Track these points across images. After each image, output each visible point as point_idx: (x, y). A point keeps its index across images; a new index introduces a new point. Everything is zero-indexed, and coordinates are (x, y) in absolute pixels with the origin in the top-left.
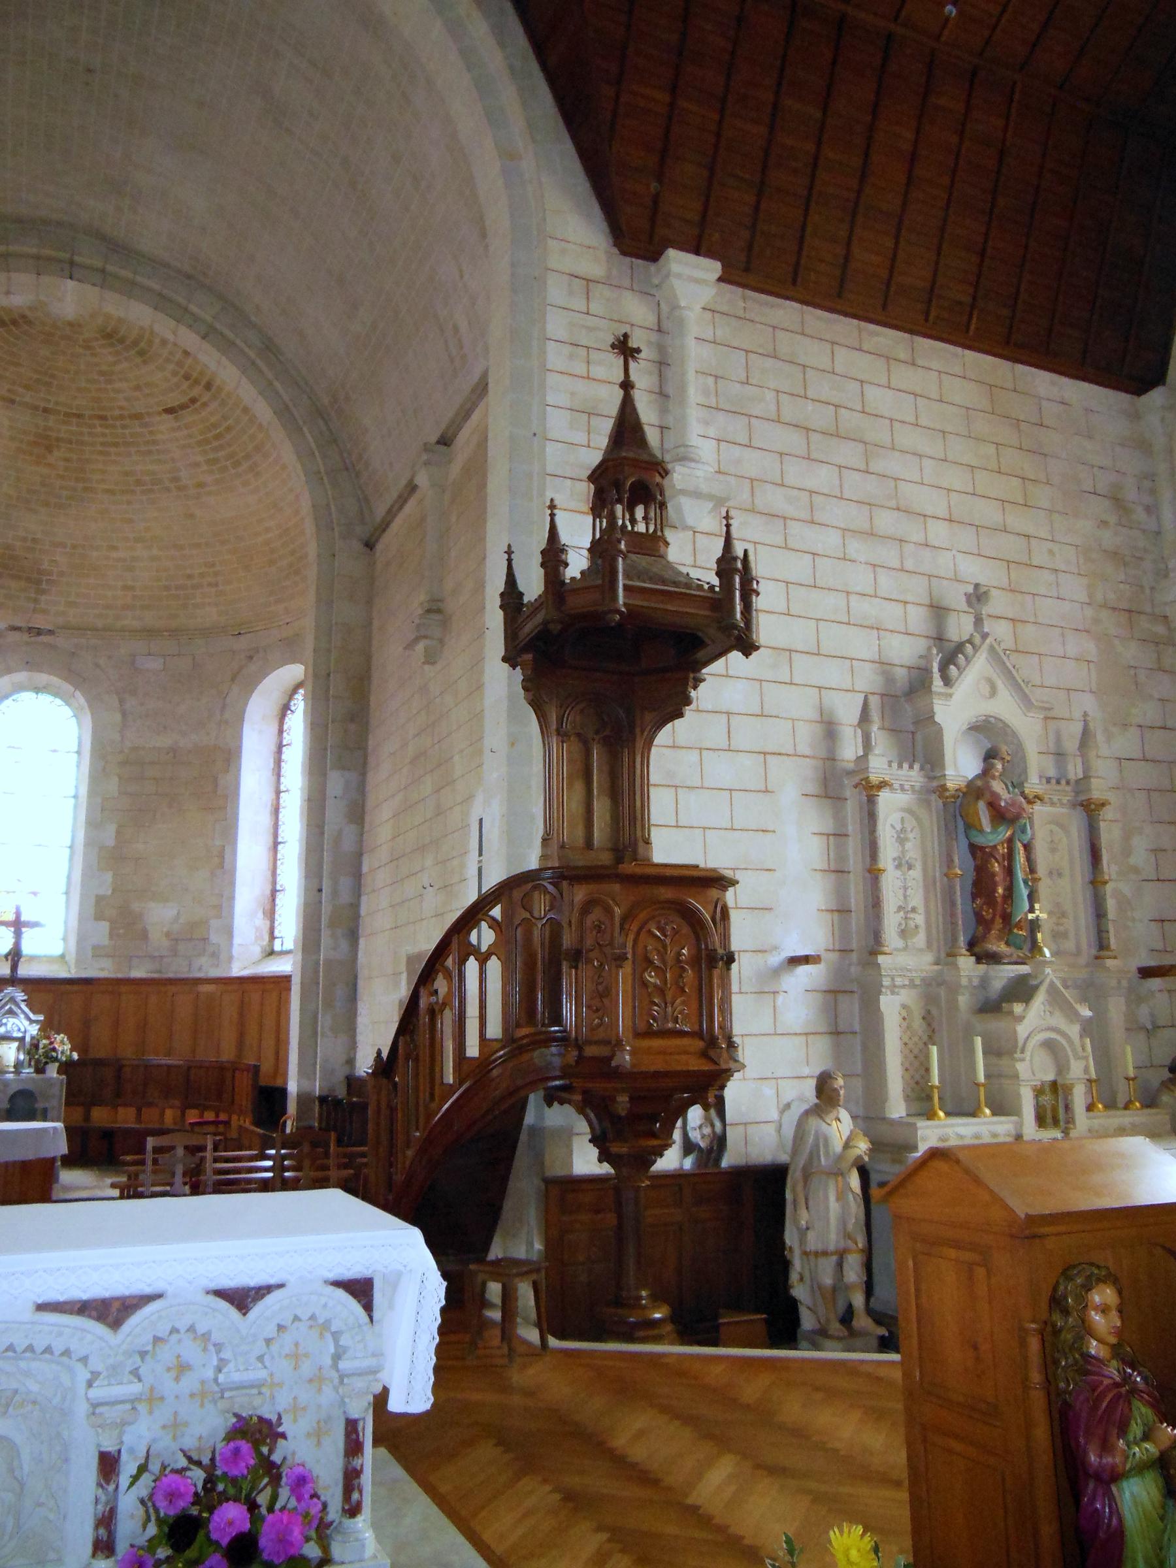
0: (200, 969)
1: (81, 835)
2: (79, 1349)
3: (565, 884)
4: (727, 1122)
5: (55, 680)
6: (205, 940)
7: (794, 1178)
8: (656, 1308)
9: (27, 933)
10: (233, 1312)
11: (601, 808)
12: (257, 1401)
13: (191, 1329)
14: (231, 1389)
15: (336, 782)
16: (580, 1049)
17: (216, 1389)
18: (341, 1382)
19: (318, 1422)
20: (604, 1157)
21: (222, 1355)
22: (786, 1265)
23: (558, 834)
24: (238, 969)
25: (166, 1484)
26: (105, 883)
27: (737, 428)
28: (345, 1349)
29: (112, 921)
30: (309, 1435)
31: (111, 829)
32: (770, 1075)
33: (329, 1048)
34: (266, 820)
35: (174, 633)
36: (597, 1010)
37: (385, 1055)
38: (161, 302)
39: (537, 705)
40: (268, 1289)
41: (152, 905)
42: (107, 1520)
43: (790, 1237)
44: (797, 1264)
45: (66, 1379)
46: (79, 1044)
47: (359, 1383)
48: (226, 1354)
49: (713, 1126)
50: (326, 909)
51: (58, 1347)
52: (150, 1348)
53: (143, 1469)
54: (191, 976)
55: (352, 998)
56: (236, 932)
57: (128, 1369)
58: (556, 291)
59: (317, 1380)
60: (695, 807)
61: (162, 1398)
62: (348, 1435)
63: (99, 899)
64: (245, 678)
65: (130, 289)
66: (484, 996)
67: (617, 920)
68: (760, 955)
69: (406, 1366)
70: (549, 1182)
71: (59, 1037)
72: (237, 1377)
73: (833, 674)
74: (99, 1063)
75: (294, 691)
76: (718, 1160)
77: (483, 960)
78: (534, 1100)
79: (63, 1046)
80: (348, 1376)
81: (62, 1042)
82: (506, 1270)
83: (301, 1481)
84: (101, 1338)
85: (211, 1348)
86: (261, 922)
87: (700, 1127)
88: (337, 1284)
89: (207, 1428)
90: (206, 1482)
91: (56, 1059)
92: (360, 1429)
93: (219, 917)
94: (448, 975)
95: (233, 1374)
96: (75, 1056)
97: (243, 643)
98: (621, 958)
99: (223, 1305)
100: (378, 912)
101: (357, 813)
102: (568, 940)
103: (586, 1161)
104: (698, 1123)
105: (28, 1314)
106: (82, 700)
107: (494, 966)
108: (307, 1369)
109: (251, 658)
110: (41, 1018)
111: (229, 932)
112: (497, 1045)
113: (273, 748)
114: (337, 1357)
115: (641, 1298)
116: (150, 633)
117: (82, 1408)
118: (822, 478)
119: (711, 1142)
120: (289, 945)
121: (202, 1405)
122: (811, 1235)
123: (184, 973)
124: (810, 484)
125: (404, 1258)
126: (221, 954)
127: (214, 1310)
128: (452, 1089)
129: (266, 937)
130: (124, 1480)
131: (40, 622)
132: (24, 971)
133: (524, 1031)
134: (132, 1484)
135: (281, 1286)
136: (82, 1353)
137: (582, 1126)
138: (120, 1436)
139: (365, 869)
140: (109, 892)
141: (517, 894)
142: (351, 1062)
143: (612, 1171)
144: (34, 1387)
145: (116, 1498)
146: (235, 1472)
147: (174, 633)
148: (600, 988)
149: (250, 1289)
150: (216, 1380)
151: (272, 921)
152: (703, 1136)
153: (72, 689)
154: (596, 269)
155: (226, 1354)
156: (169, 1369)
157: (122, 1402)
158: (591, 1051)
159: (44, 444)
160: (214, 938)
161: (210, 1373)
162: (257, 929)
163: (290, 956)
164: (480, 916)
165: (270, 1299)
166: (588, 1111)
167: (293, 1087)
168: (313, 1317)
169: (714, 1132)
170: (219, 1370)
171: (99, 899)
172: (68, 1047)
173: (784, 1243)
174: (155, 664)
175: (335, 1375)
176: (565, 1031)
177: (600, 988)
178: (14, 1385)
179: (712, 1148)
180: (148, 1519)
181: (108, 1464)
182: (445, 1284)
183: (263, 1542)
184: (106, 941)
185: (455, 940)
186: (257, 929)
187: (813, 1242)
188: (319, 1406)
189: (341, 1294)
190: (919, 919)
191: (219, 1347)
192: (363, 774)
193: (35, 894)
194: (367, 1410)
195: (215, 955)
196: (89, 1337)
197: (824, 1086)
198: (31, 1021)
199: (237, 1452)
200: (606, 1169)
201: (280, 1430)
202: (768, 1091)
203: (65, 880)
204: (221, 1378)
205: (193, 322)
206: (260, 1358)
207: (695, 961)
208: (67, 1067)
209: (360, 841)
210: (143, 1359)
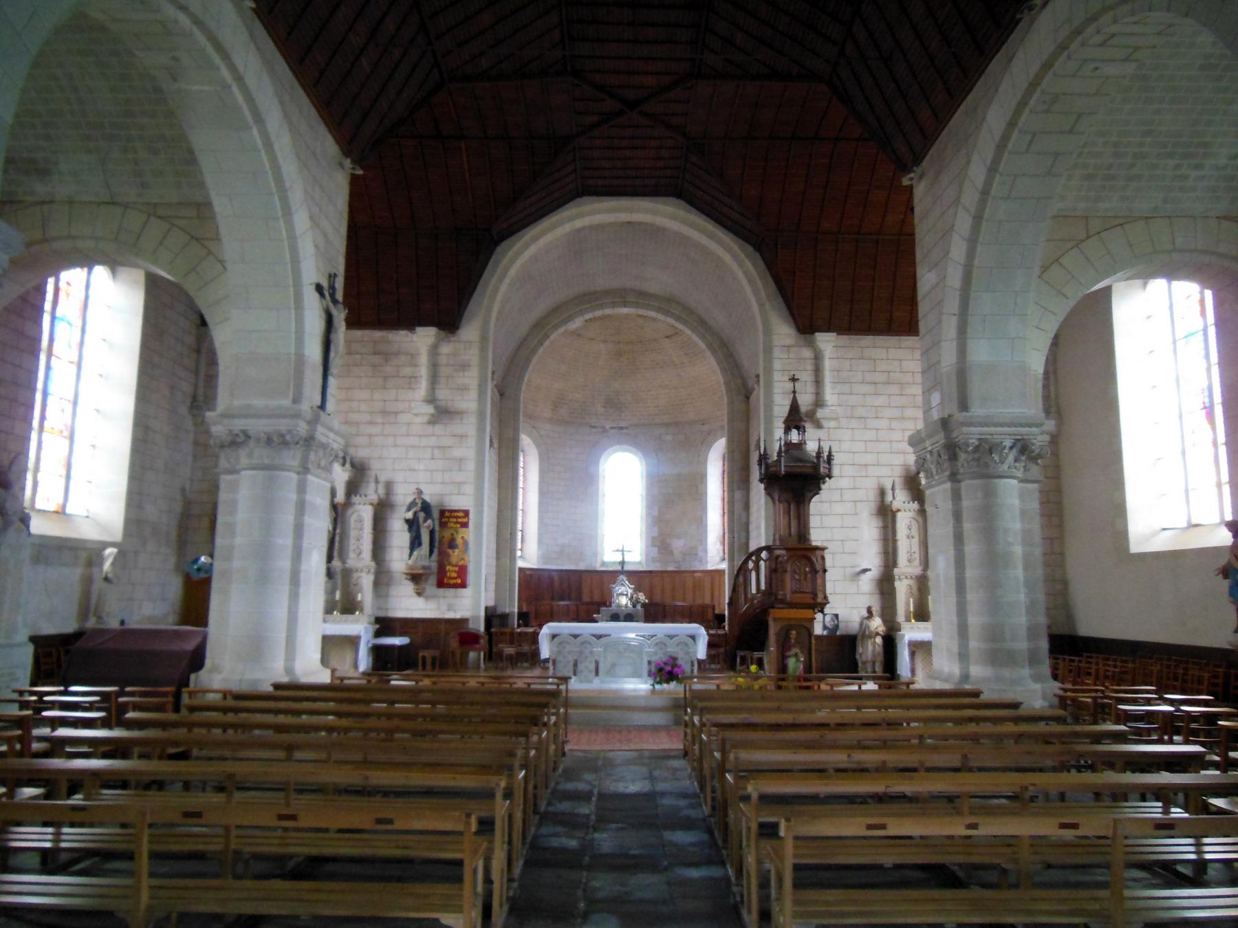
24: (710, 567)
27: (846, 388)
35: (676, 424)
38: (658, 310)
43: (858, 657)
46: (649, 596)
58: (777, 353)
60: (828, 521)
64: (707, 444)
65: (648, 307)
69: (701, 652)
73: (885, 471)
74: (656, 605)
79: (642, 597)
95: (669, 649)
97: (706, 428)
111: (705, 551)
116: (666, 425)
118: (880, 401)
124: (876, 404)
126: (703, 560)
131: (622, 424)
132: (627, 568)
147: (676, 424)
154: (790, 341)
159: (619, 354)
160: (700, 554)
171: (653, 538)
174: (669, 438)
181: (649, 663)
187: (864, 658)
190: (917, 556)
195: (701, 561)
197: (869, 610)
202: (855, 612)
205: (672, 315)
207: (811, 572)
208: (644, 605)
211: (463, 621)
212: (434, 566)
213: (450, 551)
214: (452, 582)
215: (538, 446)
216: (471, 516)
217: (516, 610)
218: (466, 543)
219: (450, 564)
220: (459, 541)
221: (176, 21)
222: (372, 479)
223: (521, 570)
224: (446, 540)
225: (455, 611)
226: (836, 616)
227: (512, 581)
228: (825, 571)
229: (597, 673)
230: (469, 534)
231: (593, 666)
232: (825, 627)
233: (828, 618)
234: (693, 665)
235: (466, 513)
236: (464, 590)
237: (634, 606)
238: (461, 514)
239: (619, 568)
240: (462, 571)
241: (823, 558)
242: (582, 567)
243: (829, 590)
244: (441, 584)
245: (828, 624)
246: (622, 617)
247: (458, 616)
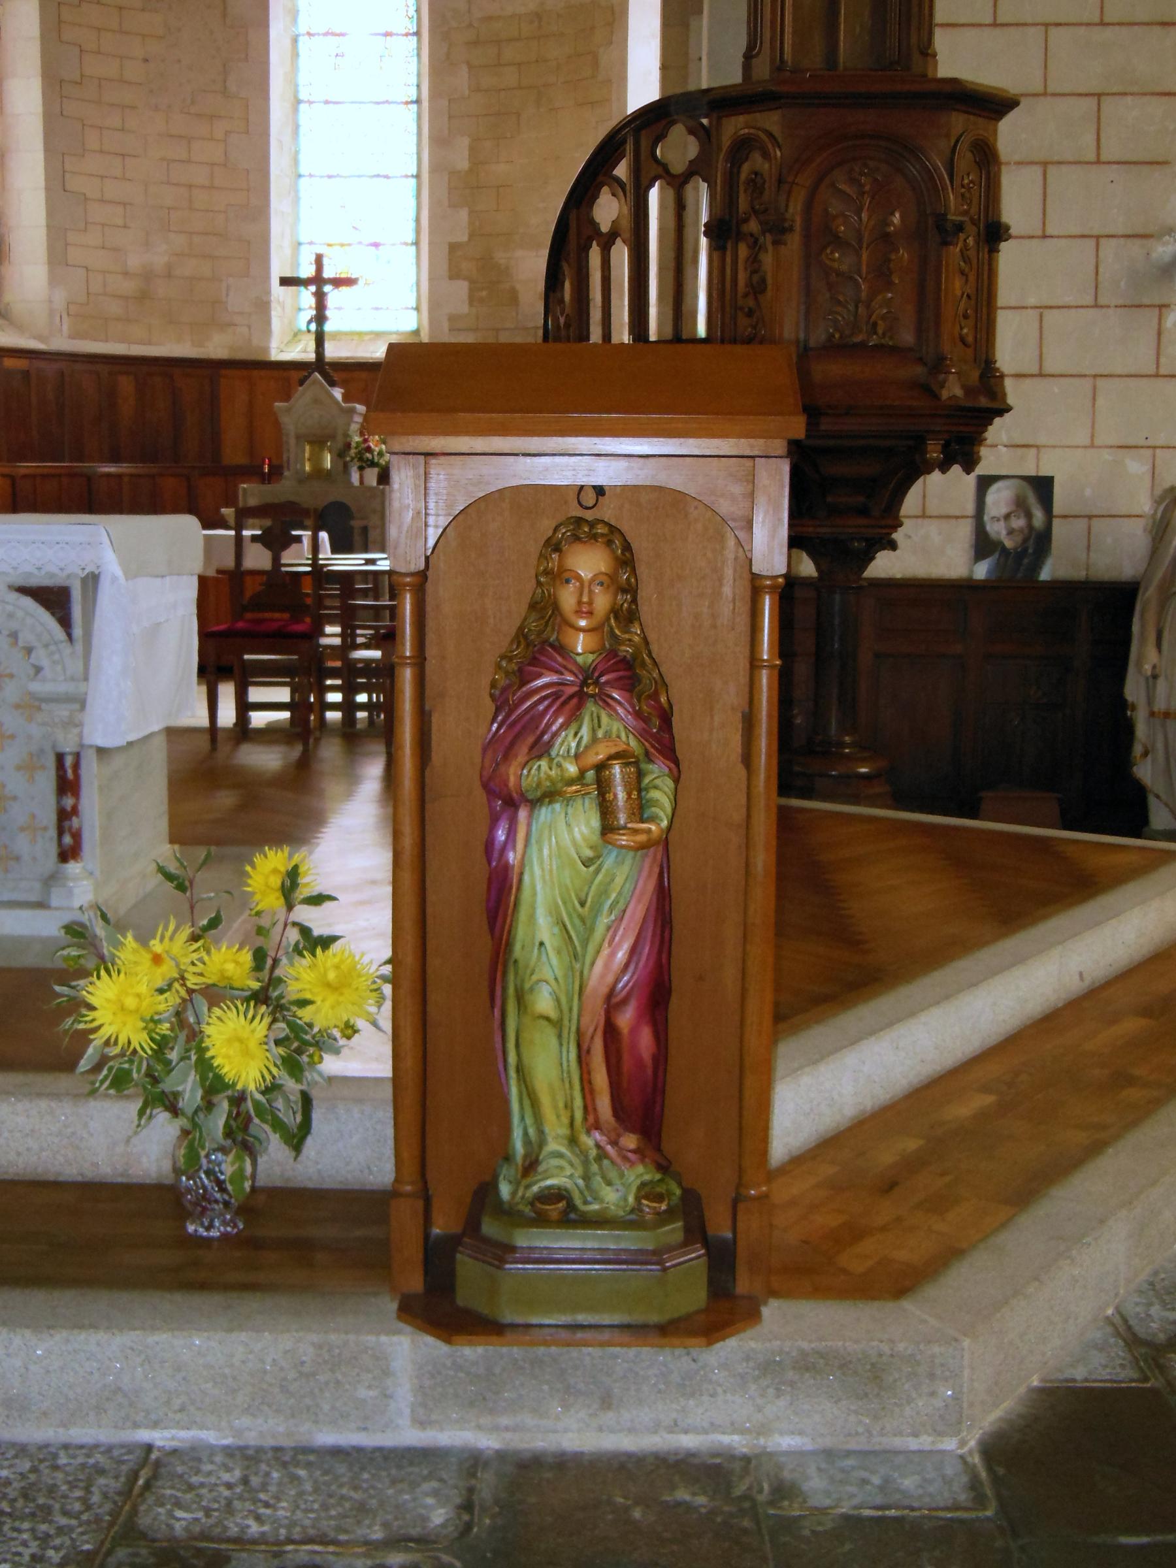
4: (1058, 508)
7: (1148, 596)
8: (863, 761)
22: (1129, 729)
26: (460, 226)
29: (472, 281)
31: (463, 144)
32: (1142, 442)
41: (519, 253)
43: (1133, 690)
44: (1141, 730)
49: (1029, 515)
63: (453, 247)
68: (1138, 242)
76: (1037, 565)
77: (607, 243)
87: (1007, 517)
88: (24, 590)
98: (779, 230)
104: (1004, 510)
115: (843, 745)
119: (1025, 540)
122: (1161, 686)
140: (465, 239)
152: (1011, 532)
164: (600, 178)
169: (1030, 526)
171: (453, 247)
173: (1126, 701)
179: (1025, 550)
184: (464, 309)
185: (573, 216)
189: (28, 602)
193: (376, 245)
202: (1136, 466)
203: (412, 225)
221: (694, 1494)
222: (856, 1512)
226: (1043, 486)
228: (995, 233)
232: (983, 545)
233: (999, 499)
241: (986, 158)
243: (1011, 349)
245: (996, 530)
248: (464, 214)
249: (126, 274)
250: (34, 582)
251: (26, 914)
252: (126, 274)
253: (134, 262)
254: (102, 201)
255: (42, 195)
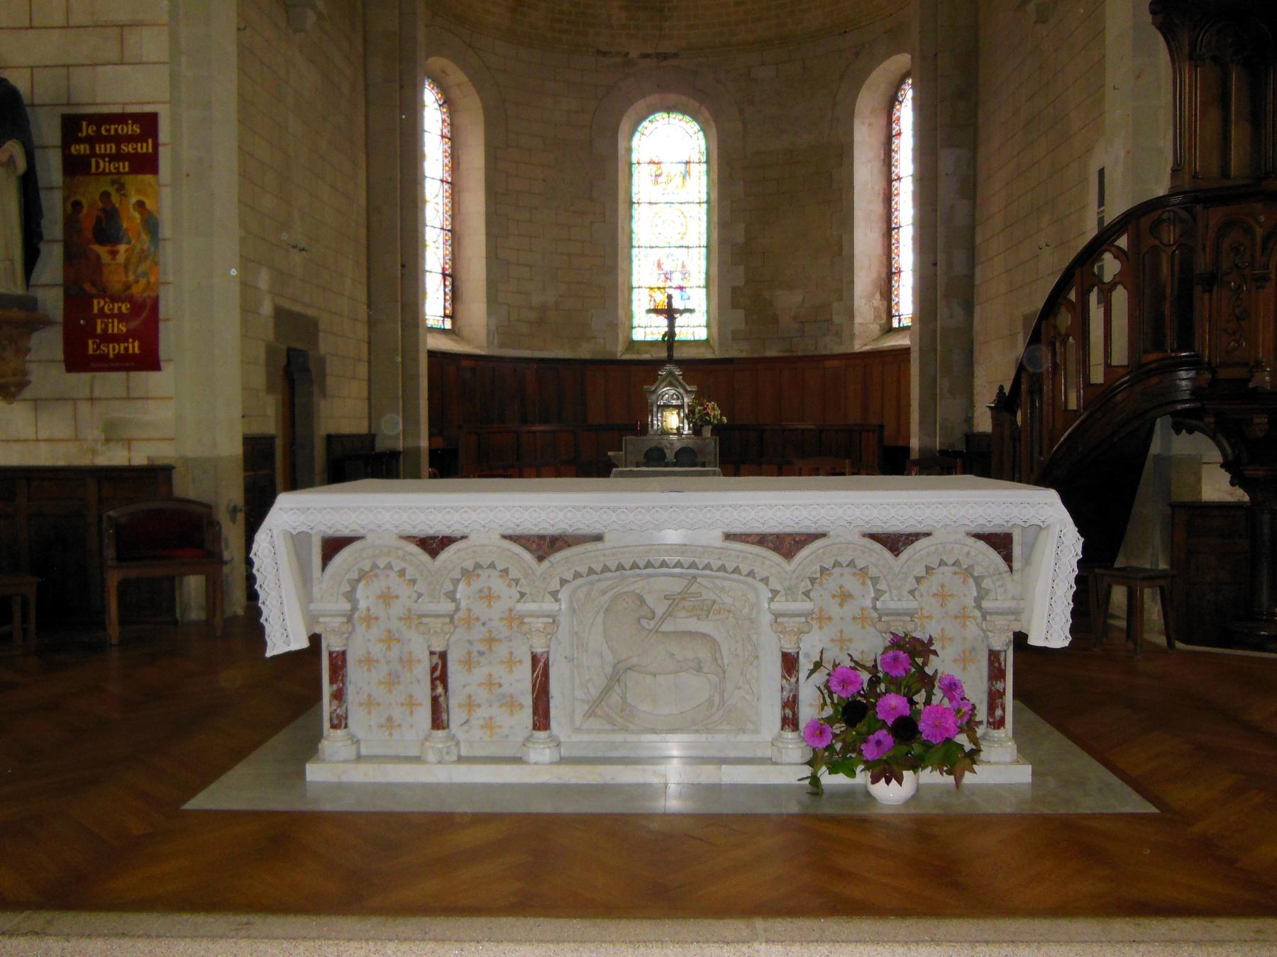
0: (825, 348)
1: (715, 235)
2: (761, 572)
3: (1199, 208)
5: (684, 99)
6: (830, 321)
9: (680, 320)
10: (887, 554)
11: (1239, 134)
12: (910, 627)
13: (851, 564)
14: (888, 615)
15: (948, 160)
16: (1214, 372)
17: (875, 615)
18: (984, 618)
19: (964, 652)
20: (1238, 479)
21: (878, 587)
23: (1190, 163)
24: (859, 346)
25: (839, 678)
28: (988, 592)
30: (955, 660)
31: (741, 227)
33: (948, 409)
34: (878, 208)
36: (1234, 333)
37: (1007, 391)
39: (1167, 30)
40: (916, 536)
42: (791, 704)
45: (751, 596)
47: (1000, 621)
48: (882, 586)
50: (941, 281)
51: (745, 569)
52: (818, 575)
53: (818, 665)
54: (816, 353)
55: (969, 363)
56: (856, 313)
57: (802, 590)
59: (962, 617)
61: (830, 619)
62: (991, 663)
66: (1110, 331)
67: (1259, 240)
70: (1176, 507)
71: (711, 405)
72: (892, 605)
75: (902, 81)
78: (1161, 426)
79: (714, 411)
80: (991, 614)
81: (713, 409)
82: (1131, 578)
83: (952, 687)
84: (779, 565)
85: (869, 582)
86: (877, 301)
88: (979, 536)
89: (869, 645)
90: (870, 680)
91: (709, 423)
92: (1002, 659)
93: (840, 299)
94: (1071, 307)
95: (889, 602)
96: (725, 420)
99: (877, 546)
100: (993, 280)
101: (970, 188)
102: (1202, 263)
103: (1217, 487)
105: (718, 542)
106: (707, 115)
107: (1120, 297)
108: (952, 606)
109: (857, 54)
110: (694, 388)
112: (1121, 371)
113: (881, 138)
114: (978, 600)
117: (766, 619)
120: (906, 322)
121: (863, 627)
123: (811, 352)
125: (1043, 515)
127: (870, 550)
128: (1076, 413)
129: (884, 316)
130: (803, 674)
132: (678, 354)
133: (1151, 357)
134: (812, 672)
135: (928, 534)
136: (765, 574)
137: (1216, 456)
138: (799, 640)
139: (978, 240)
141: (1145, 222)
142: (969, 420)
143: (1247, 498)
144: (728, 600)
145: (797, 689)
146: (894, 673)
148: (1237, 311)
149: (901, 535)
150: (875, 608)
151: (889, 300)
153: (697, 104)
155: (882, 586)
156: (834, 596)
157: (799, 615)
158: (1224, 374)
160: (837, 319)
161: (868, 603)
162: (876, 309)
163: (908, 333)
165: (920, 544)
166: (1219, 436)
167: (915, 443)
168: (956, 563)
170: (876, 599)
171: (734, 289)
172: (718, 412)
175: (978, 614)
176: (1196, 356)
177: (1237, 311)
178: (713, 597)
180: (825, 704)
181: (790, 663)
182: (1082, 540)
183: (921, 726)
184: (743, 326)
186: (876, 309)
188: (964, 639)
189: (981, 545)
191: (875, 581)
192: (974, 150)
194: (1007, 645)
195: (838, 334)
196: (767, 562)
198: (687, 392)
199: (895, 659)
200: (1240, 495)
201: (932, 648)
204: (879, 605)
206: (912, 592)
208: (718, 429)
209: (973, 216)
210: (812, 584)
211: (155, 476)
212: (52, 300)
213: (102, 251)
214: (112, 350)
215: (479, 89)
216: (164, 135)
217: (424, 443)
218: (151, 224)
219: (104, 293)
220: (131, 219)
223: (432, 354)
224: (88, 217)
225: (129, 442)
227: (410, 377)
229: (542, 718)
230: (167, 194)
231: (521, 681)
234: (996, 673)
235: (149, 123)
236: (152, 376)
237: (697, 431)
238: (132, 129)
239: (664, 355)
240: (146, 319)
242: (584, 352)
244: (77, 360)
246: (670, 456)
247: (139, 457)
248: (742, 268)
249: (531, 308)
250: (987, 530)
251: (407, 767)
252: (531, 308)
253: (536, 300)
254: (519, 264)
255: (483, 262)
